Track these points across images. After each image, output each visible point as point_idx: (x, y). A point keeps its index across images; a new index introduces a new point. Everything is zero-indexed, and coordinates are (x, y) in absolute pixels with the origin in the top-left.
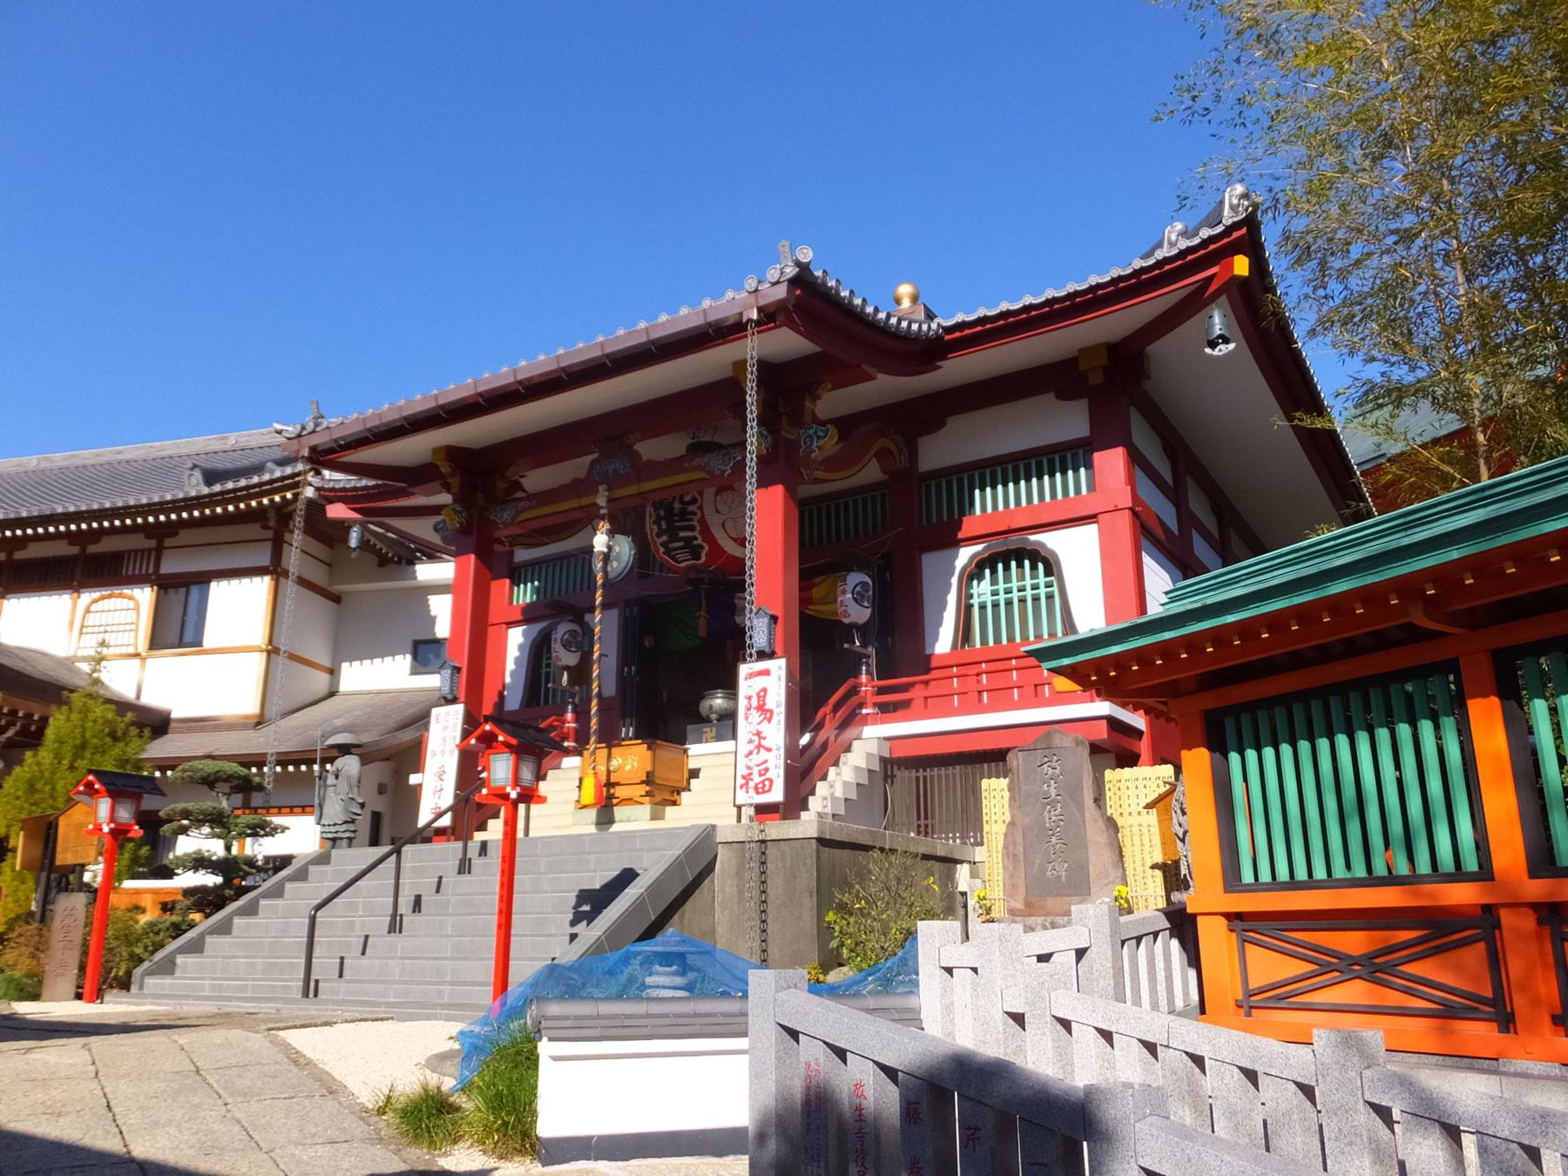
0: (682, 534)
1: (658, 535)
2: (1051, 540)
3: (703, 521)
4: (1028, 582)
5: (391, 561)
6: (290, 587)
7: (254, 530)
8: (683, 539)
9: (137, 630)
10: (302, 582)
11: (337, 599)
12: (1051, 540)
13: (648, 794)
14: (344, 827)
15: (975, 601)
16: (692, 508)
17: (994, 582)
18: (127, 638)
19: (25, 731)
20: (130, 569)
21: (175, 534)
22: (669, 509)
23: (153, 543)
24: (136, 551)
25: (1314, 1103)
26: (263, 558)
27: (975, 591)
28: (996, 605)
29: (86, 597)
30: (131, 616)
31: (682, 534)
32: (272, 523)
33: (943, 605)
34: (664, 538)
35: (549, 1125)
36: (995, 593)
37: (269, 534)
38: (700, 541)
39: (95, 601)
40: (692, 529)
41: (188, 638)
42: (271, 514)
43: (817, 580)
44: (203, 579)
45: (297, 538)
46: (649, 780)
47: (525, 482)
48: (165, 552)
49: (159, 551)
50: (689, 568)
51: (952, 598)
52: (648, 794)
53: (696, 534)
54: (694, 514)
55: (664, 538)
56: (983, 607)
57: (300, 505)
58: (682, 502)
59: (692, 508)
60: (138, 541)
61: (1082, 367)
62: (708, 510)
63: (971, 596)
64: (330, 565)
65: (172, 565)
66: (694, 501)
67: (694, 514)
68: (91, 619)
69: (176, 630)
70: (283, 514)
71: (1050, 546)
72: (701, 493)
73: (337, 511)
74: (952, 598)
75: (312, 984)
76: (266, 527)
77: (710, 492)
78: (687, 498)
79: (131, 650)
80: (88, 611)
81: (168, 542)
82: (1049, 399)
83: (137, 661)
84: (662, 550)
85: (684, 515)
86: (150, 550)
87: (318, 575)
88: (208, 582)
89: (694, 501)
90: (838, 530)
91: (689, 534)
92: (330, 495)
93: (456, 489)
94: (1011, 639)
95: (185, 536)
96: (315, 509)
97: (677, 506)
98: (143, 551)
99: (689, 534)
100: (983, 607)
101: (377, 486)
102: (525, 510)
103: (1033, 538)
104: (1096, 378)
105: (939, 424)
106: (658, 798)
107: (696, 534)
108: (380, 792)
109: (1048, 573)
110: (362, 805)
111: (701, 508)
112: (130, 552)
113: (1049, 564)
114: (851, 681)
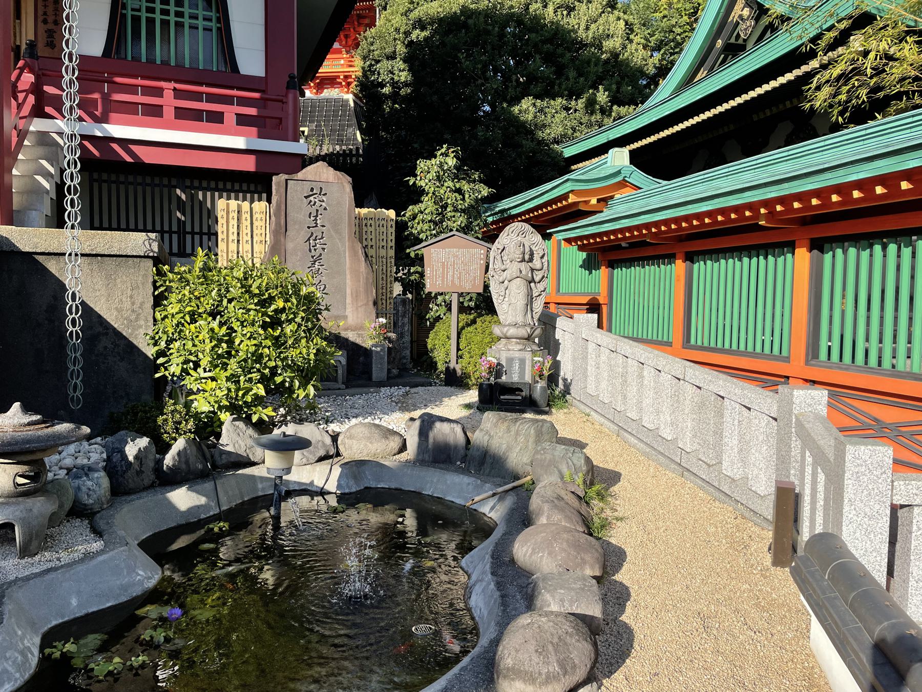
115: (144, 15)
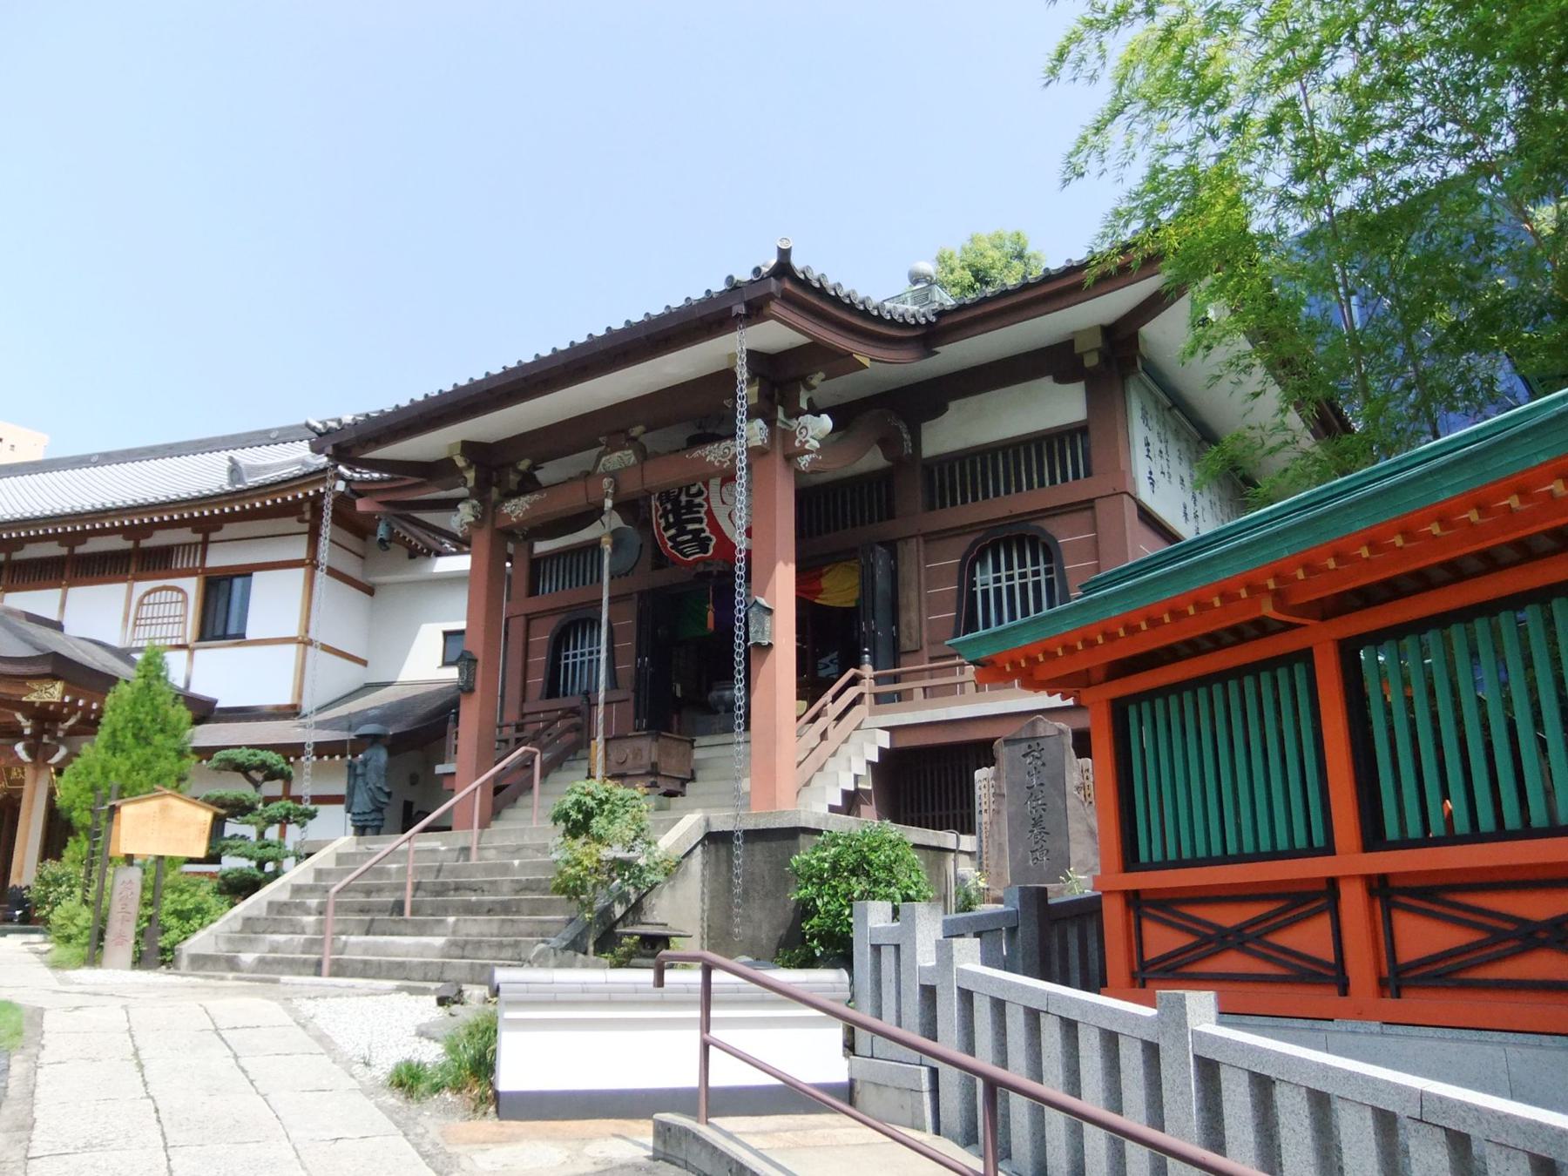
0: (690, 527)
1: (666, 529)
3: (710, 513)
4: (1029, 569)
5: (420, 553)
6: (321, 576)
7: (291, 524)
8: (691, 532)
9: (185, 623)
10: (332, 572)
11: (369, 590)
14: (373, 816)
15: (979, 589)
16: (698, 500)
17: (997, 569)
18: (176, 630)
19: (82, 721)
20: (179, 563)
21: (219, 528)
22: (676, 501)
23: (199, 537)
24: (184, 545)
26: (299, 550)
27: (978, 578)
28: (998, 591)
29: (142, 587)
30: (179, 609)
31: (690, 527)
32: (307, 516)
34: (672, 532)
35: (509, 1079)
36: (997, 580)
37: (306, 527)
38: (707, 533)
39: (155, 590)
40: (700, 521)
41: (232, 630)
42: (307, 507)
44: (246, 572)
45: (327, 530)
47: (326, 459)
48: (211, 546)
49: (205, 543)
50: (697, 561)
53: (704, 525)
54: (701, 506)
55: (672, 532)
56: (985, 593)
57: (328, 502)
58: (688, 494)
59: (698, 500)
60: (185, 535)
61: (1078, 349)
62: (715, 503)
63: (974, 584)
64: (362, 557)
65: (218, 558)
66: (700, 493)
67: (701, 506)
68: (145, 612)
69: (219, 620)
70: (316, 502)
72: (706, 484)
73: (362, 506)
76: (301, 521)
77: (715, 483)
78: (694, 490)
79: (180, 642)
80: (141, 603)
81: (213, 536)
82: (1047, 382)
83: (185, 653)
84: (670, 544)
85: (691, 506)
86: (196, 544)
87: (350, 566)
89: (700, 493)
91: (697, 526)
92: (358, 490)
93: (471, 483)
95: (229, 530)
96: (343, 504)
97: (684, 498)
98: (190, 545)
99: (697, 526)
100: (985, 593)
101: (381, 481)
103: (1033, 523)
104: (1091, 361)
105: (938, 410)
106: (663, 789)
107: (704, 525)
108: (413, 784)
109: (1048, 560)
110: (389, 795)
111: (707, 500)
112: (178, 546)
114: (851, 672)
115: (991, 587)
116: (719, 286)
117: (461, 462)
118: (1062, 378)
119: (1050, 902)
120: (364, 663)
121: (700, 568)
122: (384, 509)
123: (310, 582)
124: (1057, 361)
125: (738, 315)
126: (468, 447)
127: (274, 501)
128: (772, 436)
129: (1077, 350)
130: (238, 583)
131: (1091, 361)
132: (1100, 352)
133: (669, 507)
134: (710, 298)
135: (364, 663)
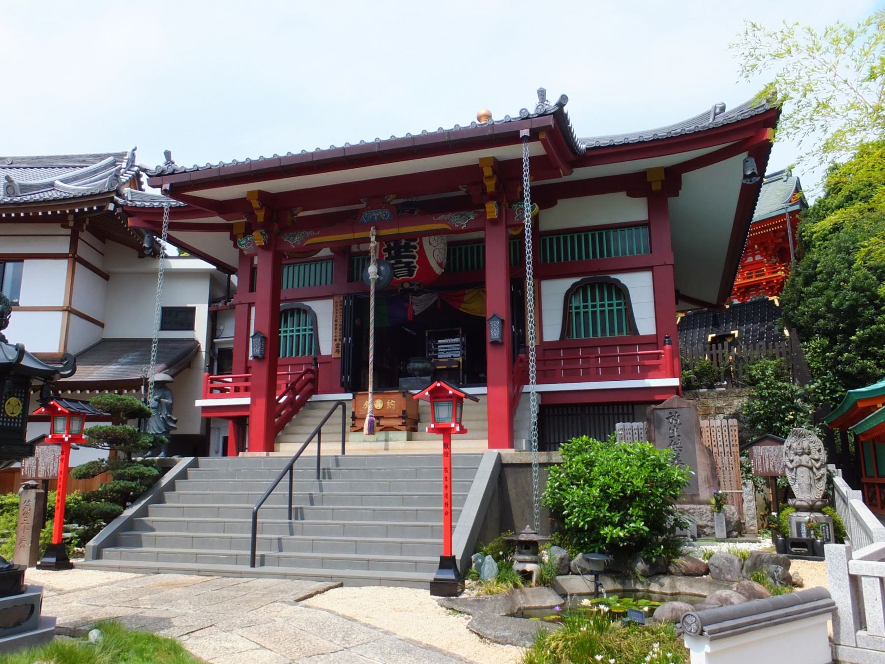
0: (404, 260)
2: (625, 279)
7: (56, 228)
11: (106, 276)
12: (625, 279)
13: (404, 424)
17: (585, 300)
25: (862, 559)
26: (65, 249)
27: (574, 305)
31: (404, 260)
32: (71, 224)
33: (139, 502)
37: (68, 231)
38: (415, 264)
42: (71, 218)
43: (467, 291)
46: (404, 416)
51: (143, 502)
52: (404, 424)
53: (415, 261)
63: (571, 308)
71: (313, 309)
74: (143, 502)
75: (321, 471)
76: (65, 226)
82: (621, 196)
88: (23, 261)
90: (467, 263)
94: (631, 251)
97: (403, 242)
102: (311, 237)
103: (613, 276)
104: (657, 187)
113: (622, 292)
116: (515, 114)
117: (256, 204)
118: (632, 194)
119: (860, 492)
120: (102, 325)
121: (406, 285)
122: (146, 225)
123: (72, 272)
124: (633, 185)
125: (525, 137)
126: (262, 195)
127: (731, 303)
128: (500, 213)
129: (649, 179)
130: (10, 266)
131: (657, 187)
132: (662, 181)
133: (392, 245)
134: (509, 122)
135: (102, 325)
